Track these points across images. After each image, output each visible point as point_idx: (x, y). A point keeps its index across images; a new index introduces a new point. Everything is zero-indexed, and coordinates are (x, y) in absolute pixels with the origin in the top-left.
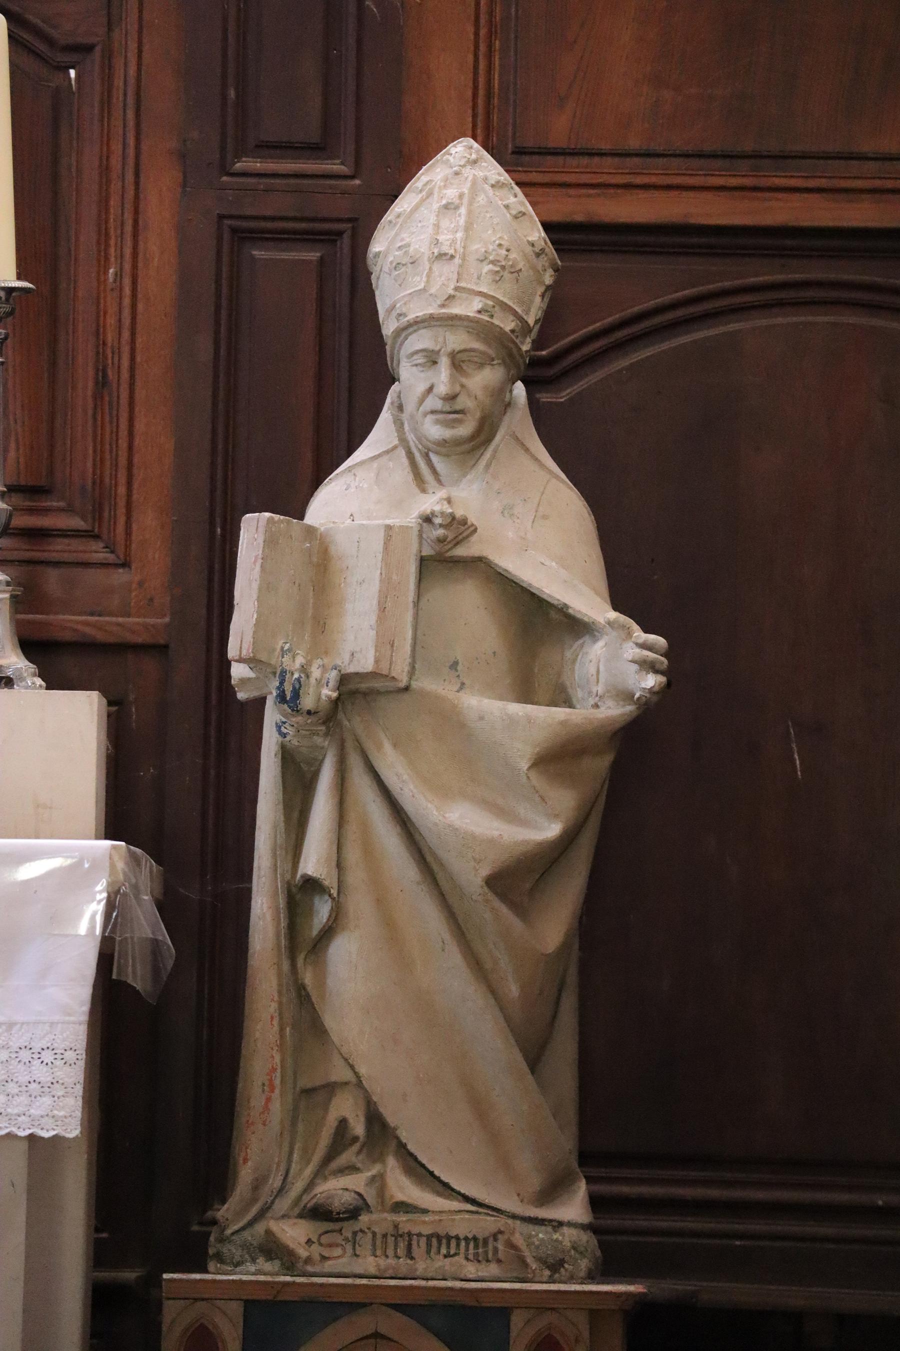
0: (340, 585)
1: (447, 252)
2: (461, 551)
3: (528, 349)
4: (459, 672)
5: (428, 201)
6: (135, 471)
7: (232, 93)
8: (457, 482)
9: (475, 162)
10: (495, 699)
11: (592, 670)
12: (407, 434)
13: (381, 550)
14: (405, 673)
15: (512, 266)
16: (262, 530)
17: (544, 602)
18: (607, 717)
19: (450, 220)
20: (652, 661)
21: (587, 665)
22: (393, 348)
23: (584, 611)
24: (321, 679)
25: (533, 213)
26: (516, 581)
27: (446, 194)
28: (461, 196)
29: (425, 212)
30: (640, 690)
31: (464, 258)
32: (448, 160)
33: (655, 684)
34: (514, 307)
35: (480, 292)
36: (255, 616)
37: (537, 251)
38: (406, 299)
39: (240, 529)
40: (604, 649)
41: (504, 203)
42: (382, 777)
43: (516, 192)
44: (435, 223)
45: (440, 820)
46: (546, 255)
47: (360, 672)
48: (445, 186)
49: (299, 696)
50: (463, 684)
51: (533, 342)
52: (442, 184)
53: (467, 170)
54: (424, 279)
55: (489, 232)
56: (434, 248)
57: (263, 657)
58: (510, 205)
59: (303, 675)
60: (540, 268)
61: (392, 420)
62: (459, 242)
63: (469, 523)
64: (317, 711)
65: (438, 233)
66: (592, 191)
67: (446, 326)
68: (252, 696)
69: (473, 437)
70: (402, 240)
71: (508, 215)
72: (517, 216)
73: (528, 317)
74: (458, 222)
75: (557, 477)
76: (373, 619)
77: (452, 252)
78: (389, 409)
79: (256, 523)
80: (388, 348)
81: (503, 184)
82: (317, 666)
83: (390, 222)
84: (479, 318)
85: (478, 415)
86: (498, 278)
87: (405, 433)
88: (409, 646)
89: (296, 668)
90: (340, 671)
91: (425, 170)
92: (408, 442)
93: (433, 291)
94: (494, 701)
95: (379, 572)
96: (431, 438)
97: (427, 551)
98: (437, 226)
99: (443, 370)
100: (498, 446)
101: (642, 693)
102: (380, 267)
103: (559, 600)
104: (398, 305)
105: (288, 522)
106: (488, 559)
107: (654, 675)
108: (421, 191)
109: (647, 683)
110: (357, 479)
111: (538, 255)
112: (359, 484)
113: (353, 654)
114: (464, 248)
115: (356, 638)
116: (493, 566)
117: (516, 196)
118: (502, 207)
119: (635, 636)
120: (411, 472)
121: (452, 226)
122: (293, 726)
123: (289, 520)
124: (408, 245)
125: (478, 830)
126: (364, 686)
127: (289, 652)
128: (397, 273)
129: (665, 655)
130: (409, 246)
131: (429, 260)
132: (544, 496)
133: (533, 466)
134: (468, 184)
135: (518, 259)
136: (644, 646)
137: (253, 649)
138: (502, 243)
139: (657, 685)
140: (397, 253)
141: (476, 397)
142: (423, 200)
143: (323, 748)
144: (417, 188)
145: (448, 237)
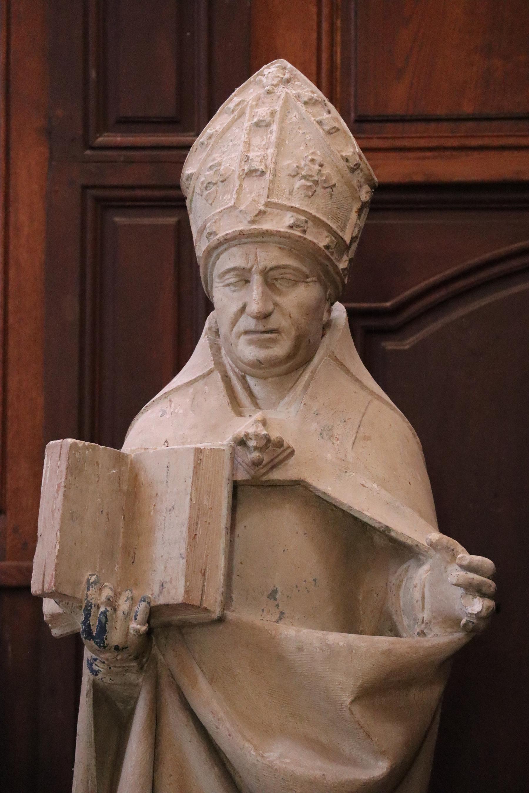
0: (149, 513)
1: (257, 168)
2: (277, 475)
3: (345, 267)
4: (278, 601)
5: (239, 121)
6: (9, 425)
7: (93, 74)
8: (274, 405)
9: (288, 81)
10: (316, 629)
11: (417, 595)
12: (224, 358)
13: (191, 474)
14: (217, 604)
15: (325, 181)
16: (64, 456)
17: (368, 527)
18: (433, 646)
19: (262, 137)
20: (478, 584)
21: (411, 590)
22: (206, 269)
23: (408, 534)
24: (129, 613)
25: (347, 129)
26: (336, 504)
27: (257, 112)
28: (273, 114)
29: (237, 131)
30: (467, 616)
31: (275, 175)
32: (261, 81)
33: (482, 610)
34: (329, 222)
35: (292, 207)
36: (58, 547)
37: (352, 166)
38: (216, 218)
39: (44, 458)
40: (429, 573)
41: (317, 119)
42: (199, 717)
43: (329, 108)
44: (246, 140)
45: (258, 761)
46: (362, 170)
47: (170, 603)
48: (257, 105)
49: (106, 630)
50: (282, 613)
51: (350, 261)
52: (254, 103)
53: (280, 89)
54: (235, 196)
55: (302, 148)
56: (244, 165)
57: (67, 591)
58: (323, 122)
59: (109, 609)
60: (355, 182)
61: (208, 345)
62: (270, 158)
63: (285, 445)
64: (126, 646)
65: (249, 151)
66: (428, 154)
67: (257, 242)
68: (65, 632)
69: (290, 357)
70: (214, 160)
71: (321, 131)
72: (331, 131)
73: (344, 234)
74: (269, 139)
75: (379, 398)
76: (182, 547)
77: (262, 168)
78: (206, 334)
79: (59, 449)
80: (201, 270)
81: (317, 101)
82: (125, 599)
83: (202, 143)
84: (291, 233)
85: (293, 333)
86: (310, 193)
87: (222, 357)
88: (222, 575)
89: (102, 601)
90: (149, 603)
91: (238, 92)
92: (223, 365)
93: (243, 207)
94: (314, 631)
95: (189, 497)
96: (246, 361)
97: (242, 476)
98: (248, 144)
99: (255, 287)
100: (316, 368)
101: (469, 620)
102: (192, 189)
103: (380, 523)
104: (208, 225)
105: (94, 449)
106: (306, 482)
107: (481, 600)
108: (233, 111)
109: (473, 608)
110: (173, 405)
111: (353, 170)
112: (174, 410)
113: (163, 585)
114: (275, 163)
115: (165, 567)
116: (312, 489)
117: (329, 112)
118: (315, 122)
119: (460, 558)
120: (226, 396)
121: (264, 143)
122: (104, 663)
123: (95, 446)
124: (220, 164)
125: (299, 771)
126: (177, 618)
127: (95, 585)
128: (207, 192)
129: (494, 577)
130: (220, 165)
131: (239, 177)
132: (365, 417)
133: (353, 387)
134: (281, 102)
135: (332, 174)
136: (469, 568)
137: (55, 583)
138: (315, 158)
139: (484, 610)
140: (208, 173)
141: (290, 315)
142: (234, 120)
143: (137, 685)
144: (230, 109)
145: (259, 153)
